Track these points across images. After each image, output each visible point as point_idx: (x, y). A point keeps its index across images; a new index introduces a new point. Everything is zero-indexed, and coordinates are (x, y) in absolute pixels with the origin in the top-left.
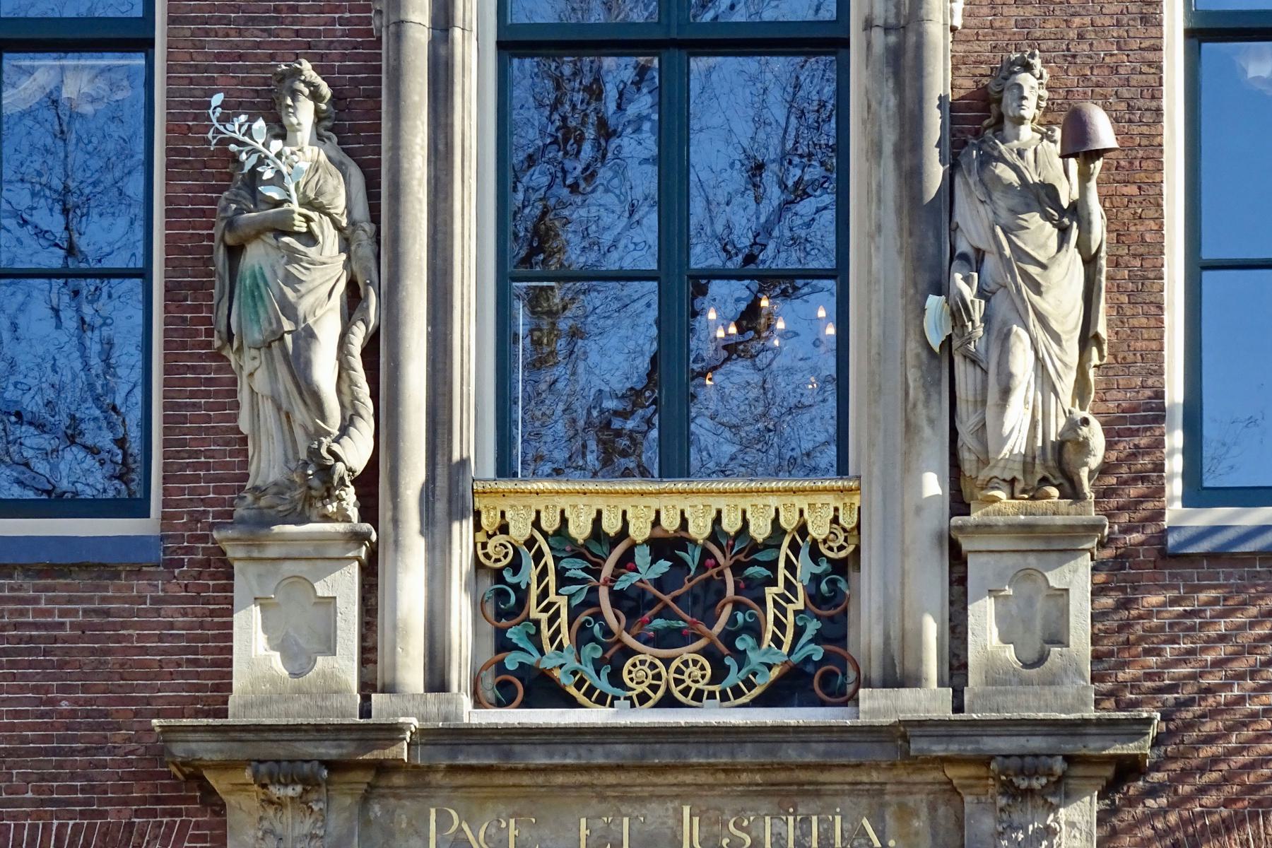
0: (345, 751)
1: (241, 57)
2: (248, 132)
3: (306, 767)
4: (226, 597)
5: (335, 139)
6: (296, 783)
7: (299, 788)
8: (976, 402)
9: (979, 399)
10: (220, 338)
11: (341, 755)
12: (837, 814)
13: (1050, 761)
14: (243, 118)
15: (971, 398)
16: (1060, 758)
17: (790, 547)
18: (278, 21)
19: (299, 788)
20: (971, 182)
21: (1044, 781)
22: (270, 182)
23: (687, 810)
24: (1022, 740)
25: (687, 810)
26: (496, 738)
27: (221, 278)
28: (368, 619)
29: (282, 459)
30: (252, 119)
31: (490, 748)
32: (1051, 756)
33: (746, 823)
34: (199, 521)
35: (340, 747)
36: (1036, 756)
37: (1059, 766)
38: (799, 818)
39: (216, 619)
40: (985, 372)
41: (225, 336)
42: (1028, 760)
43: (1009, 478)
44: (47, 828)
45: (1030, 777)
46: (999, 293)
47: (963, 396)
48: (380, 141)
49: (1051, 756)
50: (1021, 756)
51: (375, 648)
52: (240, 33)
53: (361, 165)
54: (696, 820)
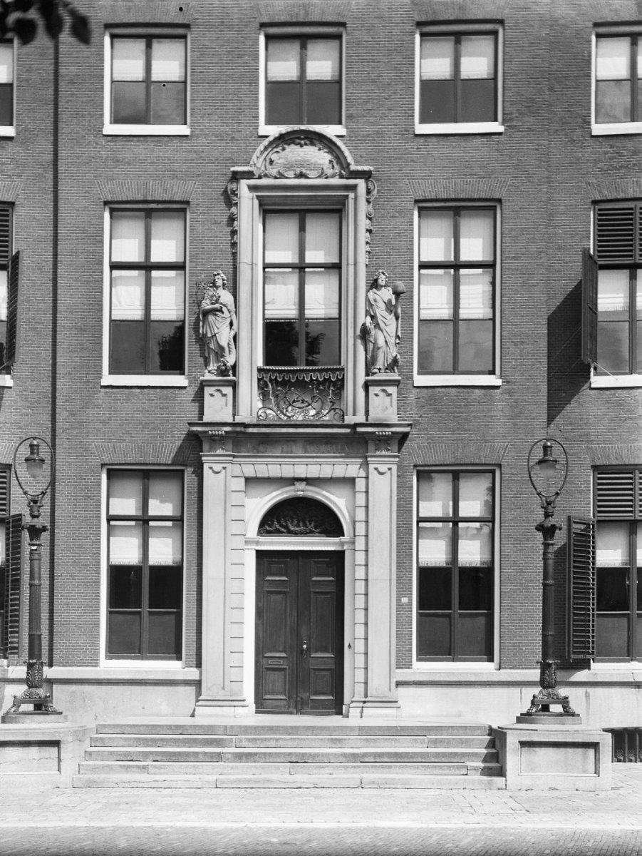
44: (169, 446)
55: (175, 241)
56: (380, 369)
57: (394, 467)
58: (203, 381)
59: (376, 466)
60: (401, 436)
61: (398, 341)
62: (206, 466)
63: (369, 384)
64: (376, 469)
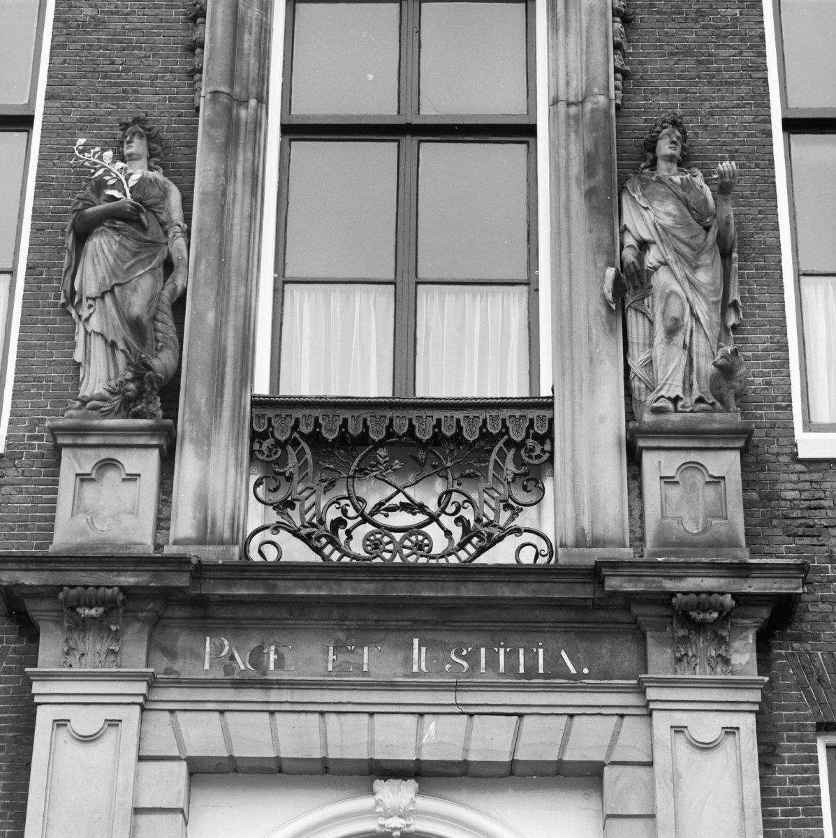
0: (140, 579)
1: (95, 121)
2: (100, 158)
3: (109, 591)
4: (54, 480)
5: (161, 170)
6: (100, 606)
7: (101, 610)
8: (645, 344)
9: (647, 342)
10: (65, 297)
11: (138, 582)
12: (541, 647)
13: (721, 598)
14: (97, 149)
15: (641, 341)
16: (730, 595)
17: (498, 454)
18: (124, 99)
19: (101, 610)
20: (636, 196)
21: (715, 615)
22: (113, 187)
23: (416, 641)
24: (698, 580)
25: (416, 641)
26: (264, 574)
27: (70, 253)
28: (164, 497)
29: (105, 379)
30: (103, 150)
31: (259, 581)
32: (723, 594)
33: (465, 652)
34: (37, 425)
35: (137, 576)
36: (710, 593)
37: (728, 600)
38: (508, 650)
39: (45, 497)
40: (652, 323)
41: (68, 295)
42: (703, 596)
43: (673, 396)
45: (704, 611)
46: (660, 269)
47: (635, 341)
48: (198, 124)
49: (723, 594)
50: (698, 593)
51: (168, 519)
52: (96, 106)
53: (181, 189)
54: (424, 649)
55: (607, 589)
56: (676, 400)
57: (747, 724)
58: (54, 431)
59: (680, 719)
60: (765, 613)
61: (732, 320)
62: (44, 717)
63: (641, 443)
64: (678, 730)
